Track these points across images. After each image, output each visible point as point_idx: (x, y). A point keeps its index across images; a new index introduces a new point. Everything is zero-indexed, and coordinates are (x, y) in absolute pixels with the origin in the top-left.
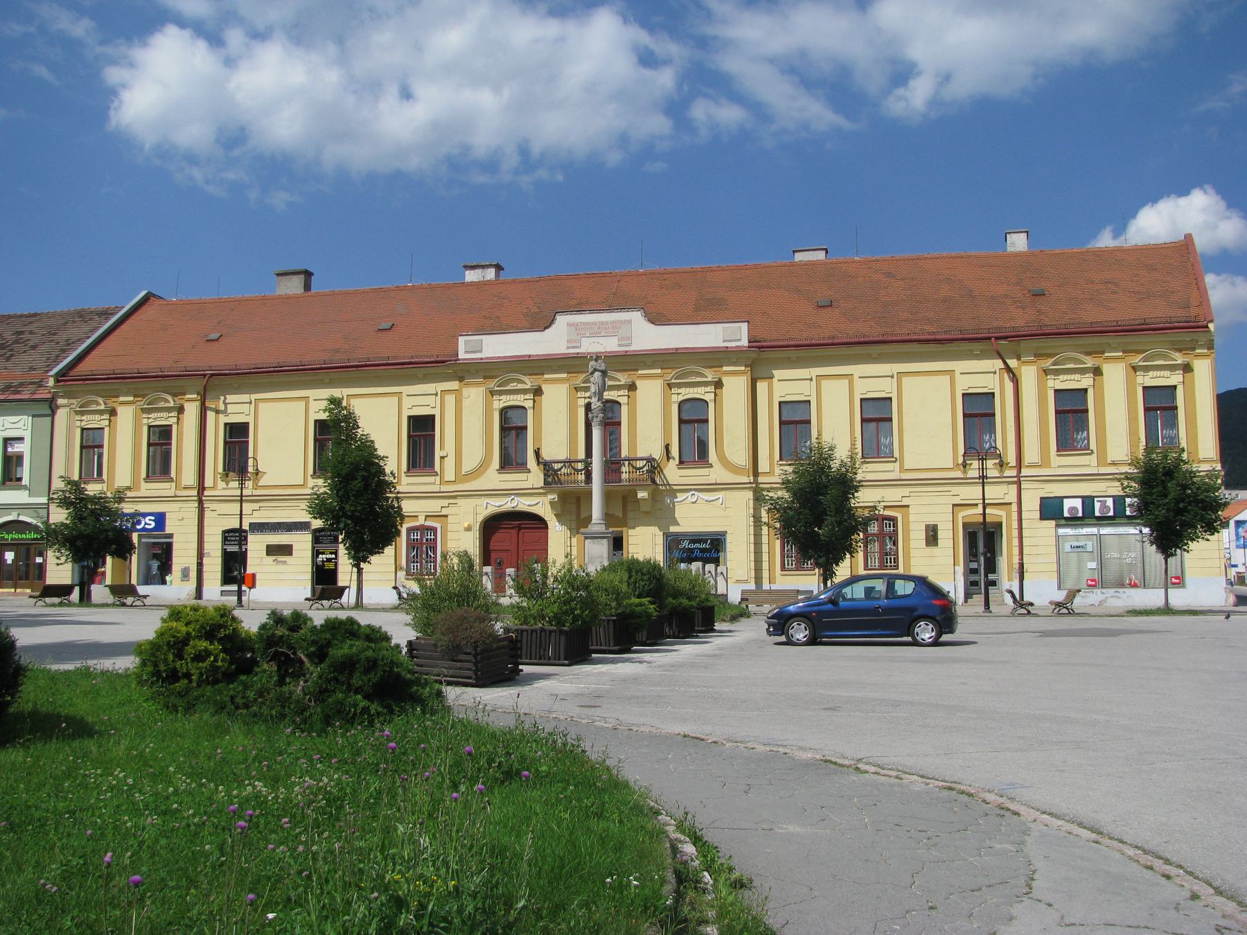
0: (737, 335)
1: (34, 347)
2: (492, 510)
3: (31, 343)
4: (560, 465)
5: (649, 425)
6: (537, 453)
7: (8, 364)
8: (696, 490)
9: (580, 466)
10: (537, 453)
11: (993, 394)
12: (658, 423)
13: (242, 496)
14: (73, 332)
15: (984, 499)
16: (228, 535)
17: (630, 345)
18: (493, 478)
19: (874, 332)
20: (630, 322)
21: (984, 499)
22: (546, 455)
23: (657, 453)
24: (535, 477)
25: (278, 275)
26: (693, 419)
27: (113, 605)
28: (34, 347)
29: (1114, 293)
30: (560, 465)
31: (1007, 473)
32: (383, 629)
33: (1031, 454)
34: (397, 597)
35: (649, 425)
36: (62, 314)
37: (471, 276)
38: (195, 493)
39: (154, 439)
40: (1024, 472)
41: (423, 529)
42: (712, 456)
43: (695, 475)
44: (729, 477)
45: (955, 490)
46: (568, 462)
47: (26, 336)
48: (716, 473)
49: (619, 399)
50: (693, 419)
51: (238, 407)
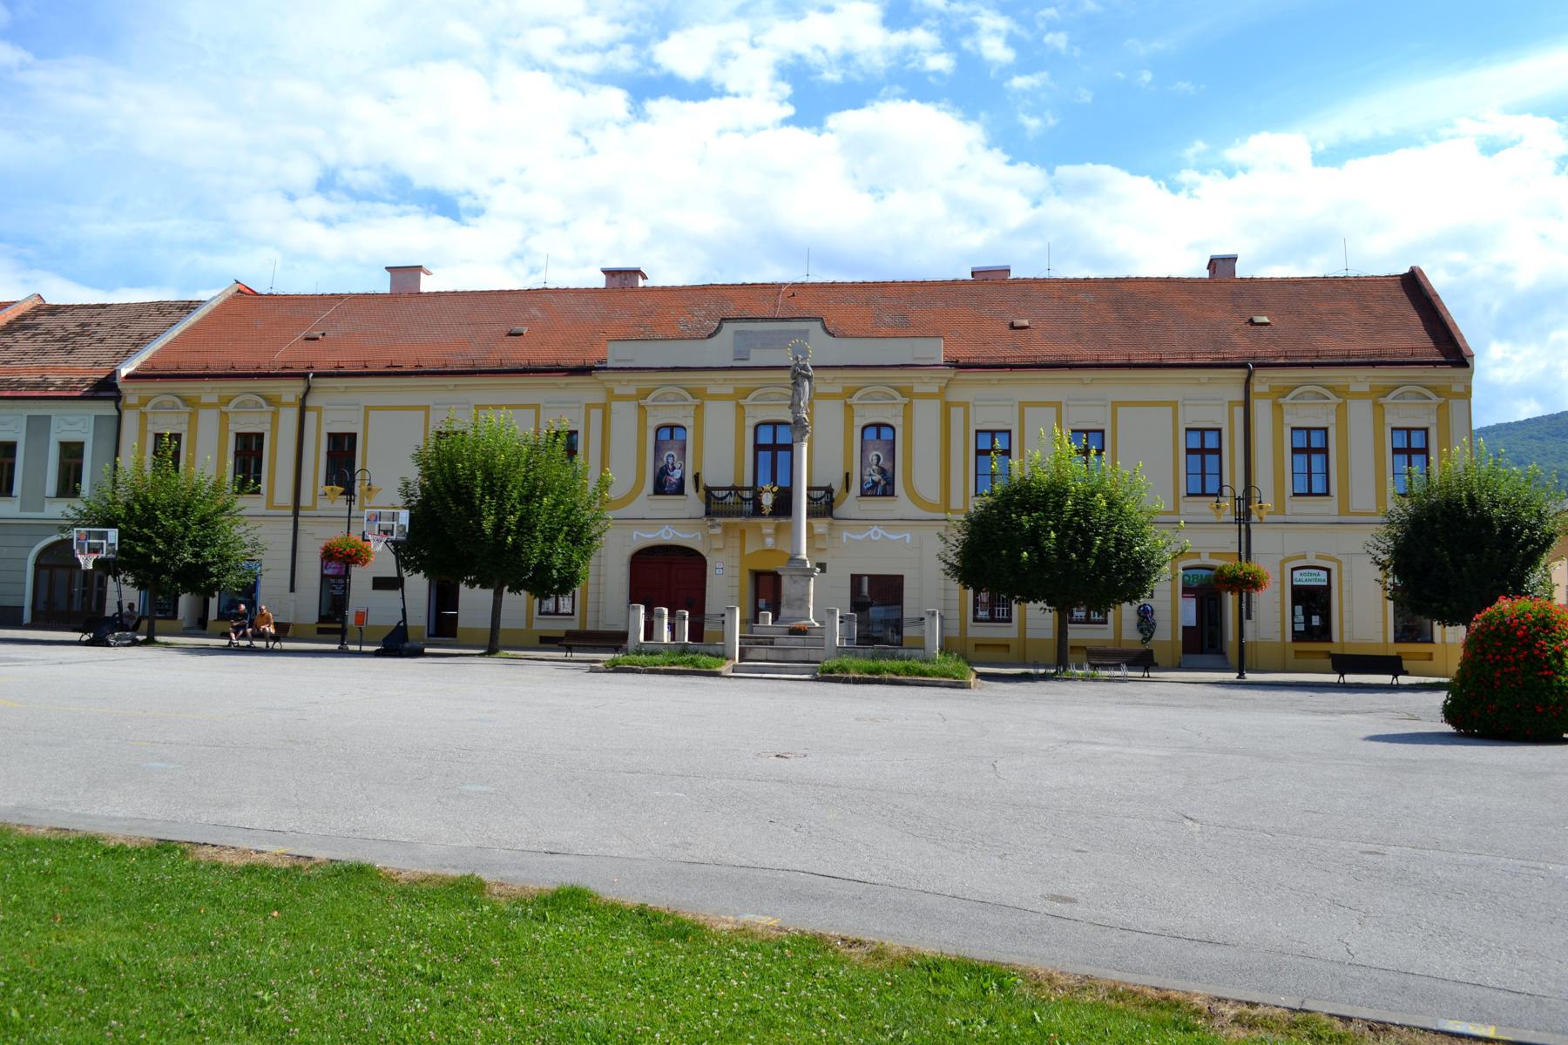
0: (936, 351)
1: (101, 341)
3: (97, 336)
4: (724, 493)
6: (697, 477)
7: (70, 358)
9: (747, 495)
10: (697, 477)
14: (147, 326)
16: (329, 555)
18: (646, 503)
19: (1087, 354)
20: (806, 332)
22: (709, 479)
24: (692, 502)
28: (101, 341)
30: (724, 493)
32: (808, 930)
37: (1265, 319)
38: (290, 512)
40: (301, 513)
43: (877, 506)
44: (913, 511)
46: (735, 489)
47: (93, 328)
48: (901, 504)
51: (337, 409)
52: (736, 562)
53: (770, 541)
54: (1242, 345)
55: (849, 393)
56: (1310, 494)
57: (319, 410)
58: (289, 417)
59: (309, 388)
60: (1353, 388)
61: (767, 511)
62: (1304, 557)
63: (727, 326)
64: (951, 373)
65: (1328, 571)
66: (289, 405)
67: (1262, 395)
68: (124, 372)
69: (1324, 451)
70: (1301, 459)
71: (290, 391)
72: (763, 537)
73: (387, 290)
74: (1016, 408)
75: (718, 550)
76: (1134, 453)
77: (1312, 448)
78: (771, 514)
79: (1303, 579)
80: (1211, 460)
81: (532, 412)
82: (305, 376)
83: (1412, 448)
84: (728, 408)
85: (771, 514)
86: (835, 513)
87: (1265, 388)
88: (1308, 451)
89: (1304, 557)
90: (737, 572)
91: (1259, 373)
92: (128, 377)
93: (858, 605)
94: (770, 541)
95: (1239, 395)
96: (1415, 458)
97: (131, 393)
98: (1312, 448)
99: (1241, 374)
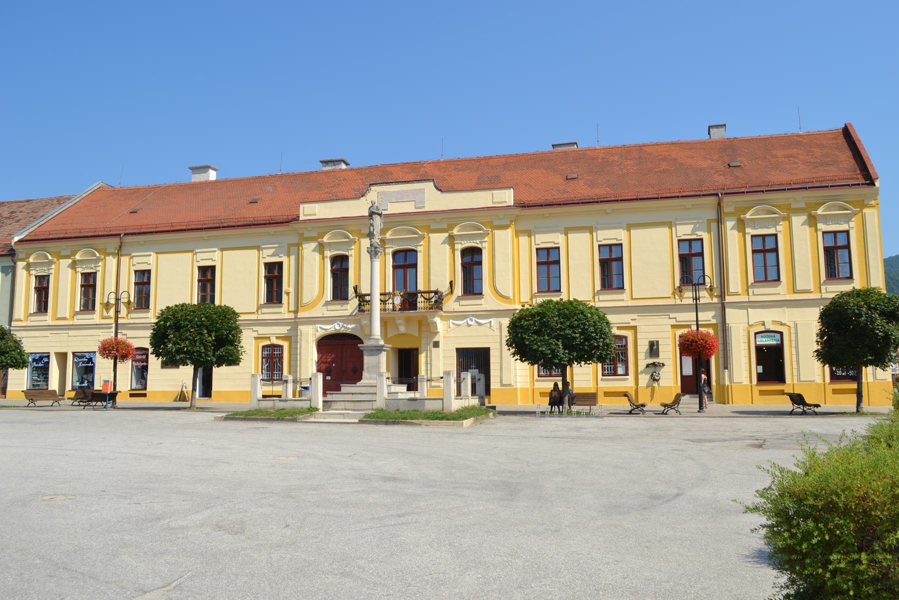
2: (321, 333)
5: (439, 267)
6: (355, 288)
8: (473, 315)
11: (621, 245)
12: (528, 260)
13: (296, 318)
15: (697, 320)
17: (424, 207)
21: (697, 320)
23: (444, 288)
25: (192, 169)
26: (472, 259)
27: (791, 413)
29: (795, 163)
31: (685, 302)
33: (735, 282)
34: (629, 404)
35: (439, 267)
36: (37, 201)
40: (728, 299)
42: (486, 288)
50: (472, 259)
51: (147, 260)
53: (402, 329)
54: (721, 180)
56: (766, 280)
60: (793, 206)
62: (269, 338)
63: (373, 188)
64: (518, 211)
65: (781, 333)
67: (730, 214)
68: (16, 239)
69: (776, 250)
70: (760, 256)
72: (397, 326)
74: (286, 246)
77: (766, 249)
78: (400, 310)
79: (763, 341)
80: (771, 257)
87: (732, 210)
88: (764, 251)
89: (269, 338)
91: (727, 200)
92: (19, 241)
95: (713, 215)
96: (769, 255)
97: (18, 248)
98: (766, 249)
99: (713, 200)
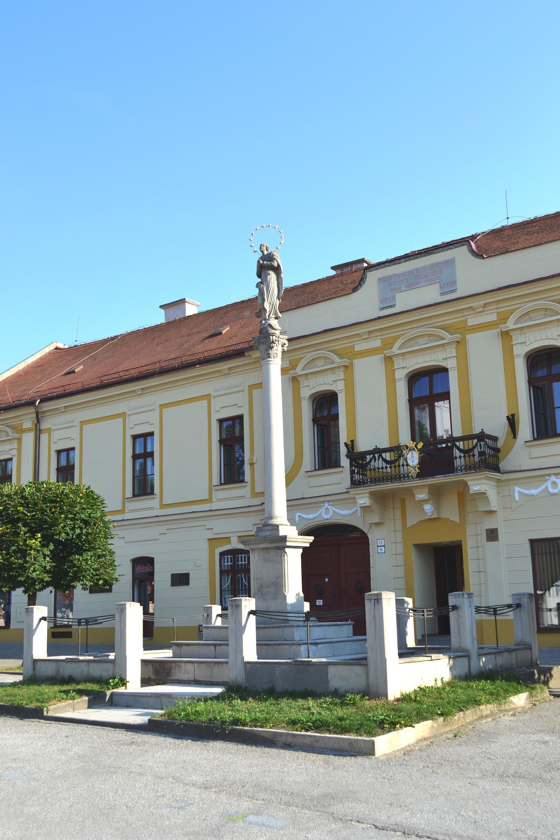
8: (328, 501)
39: (423, 389)
41: (234, 552)
45: (209, 523)
49: (444, 364)
52: (399, 537)
55: (503, 319)
57: (49, 431)
58: (28, 439)
59: (37, 413)
61: (414, 472)
65: (222, 554)
66: (28, 430)
71: (26, 419)
73: (163, 321)
75: (377, 524)
76: (497, 244)
81: (205, 402)
82: (31, 403)
83: (470, 595)
84: (377, 361)
85: (420, 476)
86: (503, 465)
90: (400, 548)
93: (476, 609)
94: (428, 508)
